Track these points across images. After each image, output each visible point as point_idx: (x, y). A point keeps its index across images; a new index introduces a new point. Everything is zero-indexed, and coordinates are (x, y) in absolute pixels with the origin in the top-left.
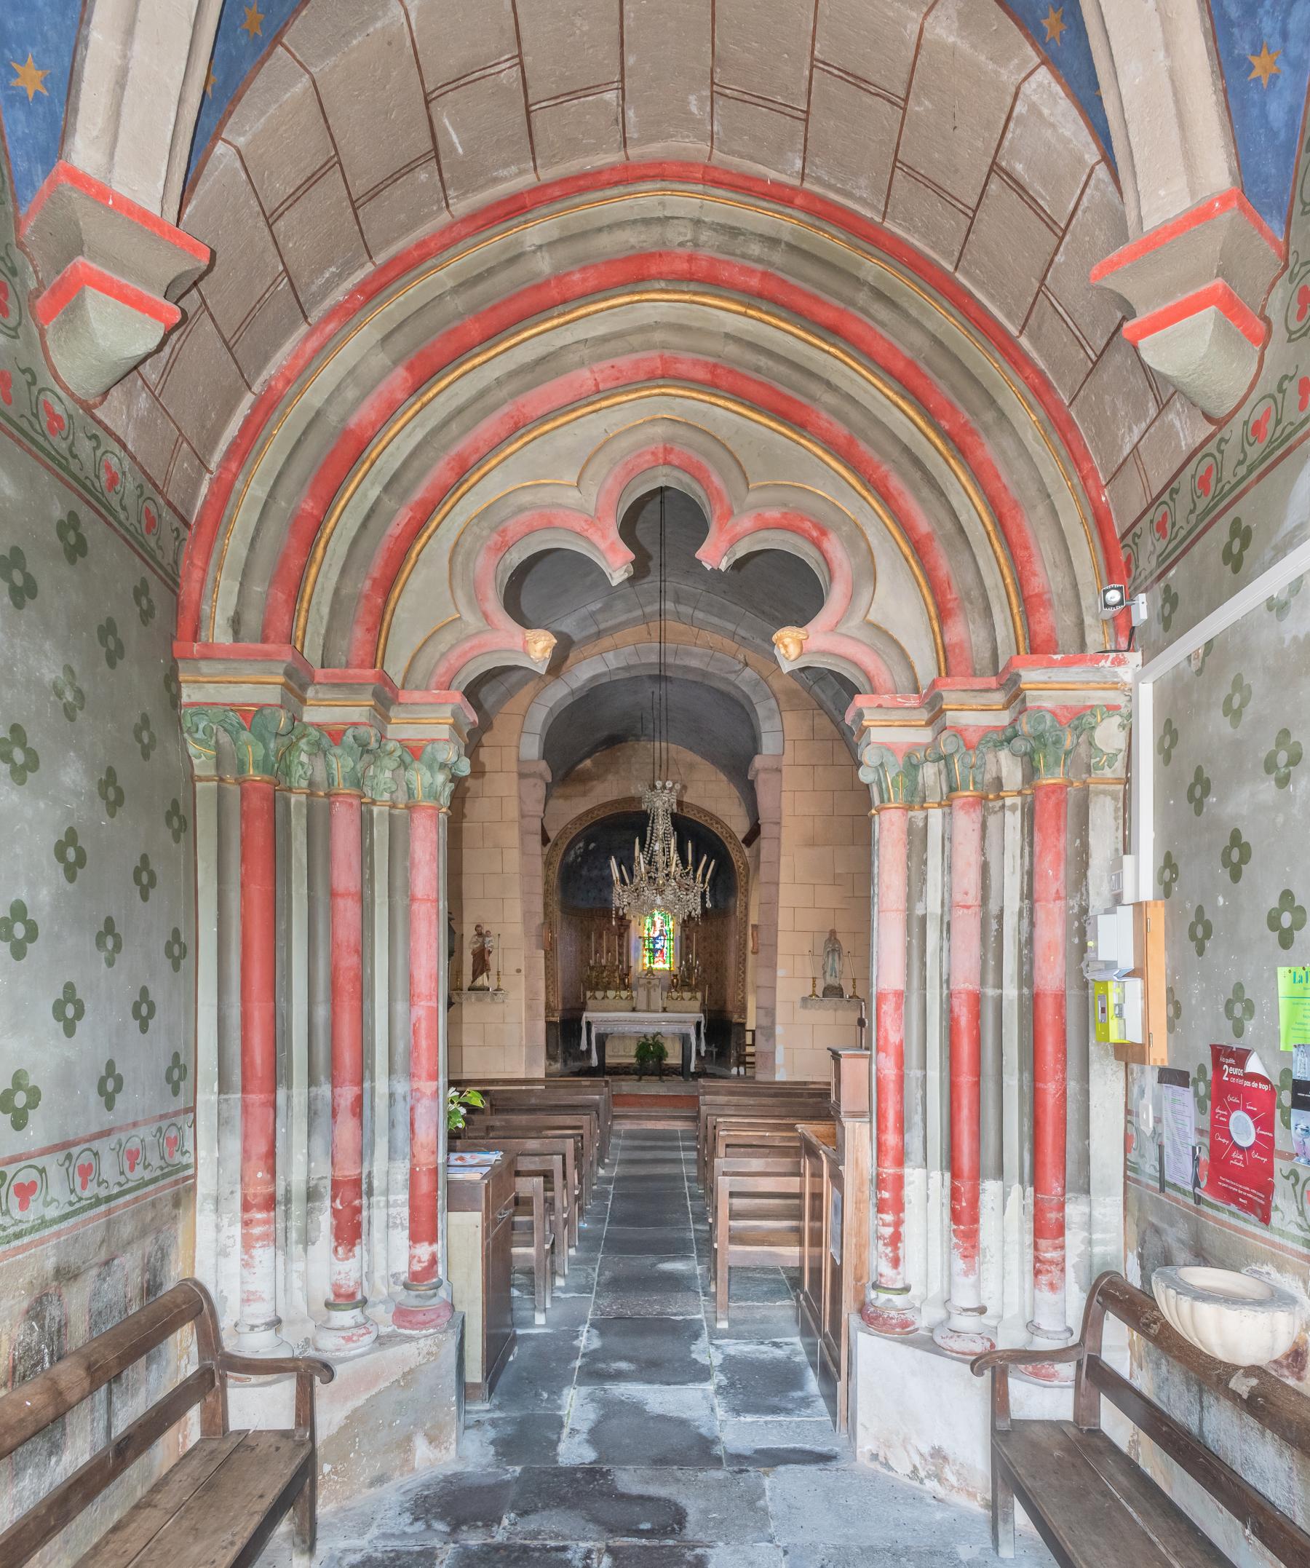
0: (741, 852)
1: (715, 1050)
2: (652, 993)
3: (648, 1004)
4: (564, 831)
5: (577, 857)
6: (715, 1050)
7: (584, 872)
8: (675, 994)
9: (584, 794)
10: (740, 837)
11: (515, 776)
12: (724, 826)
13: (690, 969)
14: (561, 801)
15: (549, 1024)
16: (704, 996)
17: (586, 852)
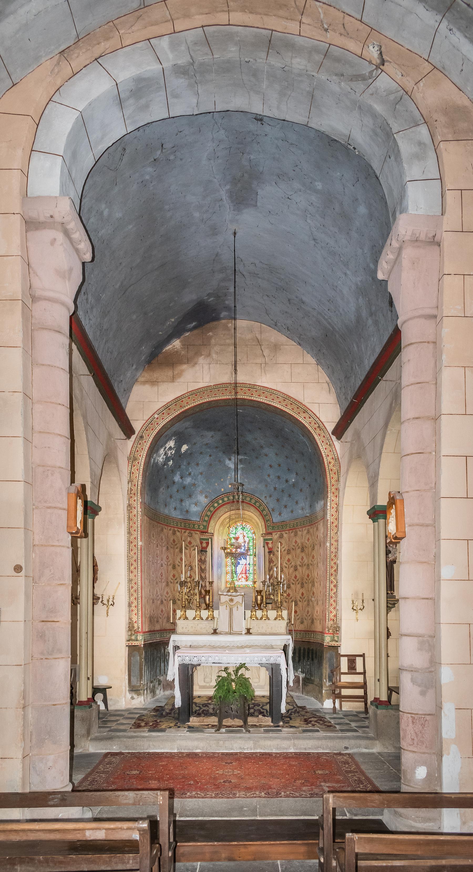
0: (331, 445)
1: (302, 676)
2: (234, 609)
3: (231, 626)
4: (150, 423)
5: (168, 459)
6: (302, 676)
7: (177, 478)
8: (259, 613)
9: (173, 379)
10: (330, 427)
11: (17, 221)
12: (313, 416)
13: (275, 584)
14: (147, 387)
15: (132, 649)
16: (289, 615)
17: (178, 456)
